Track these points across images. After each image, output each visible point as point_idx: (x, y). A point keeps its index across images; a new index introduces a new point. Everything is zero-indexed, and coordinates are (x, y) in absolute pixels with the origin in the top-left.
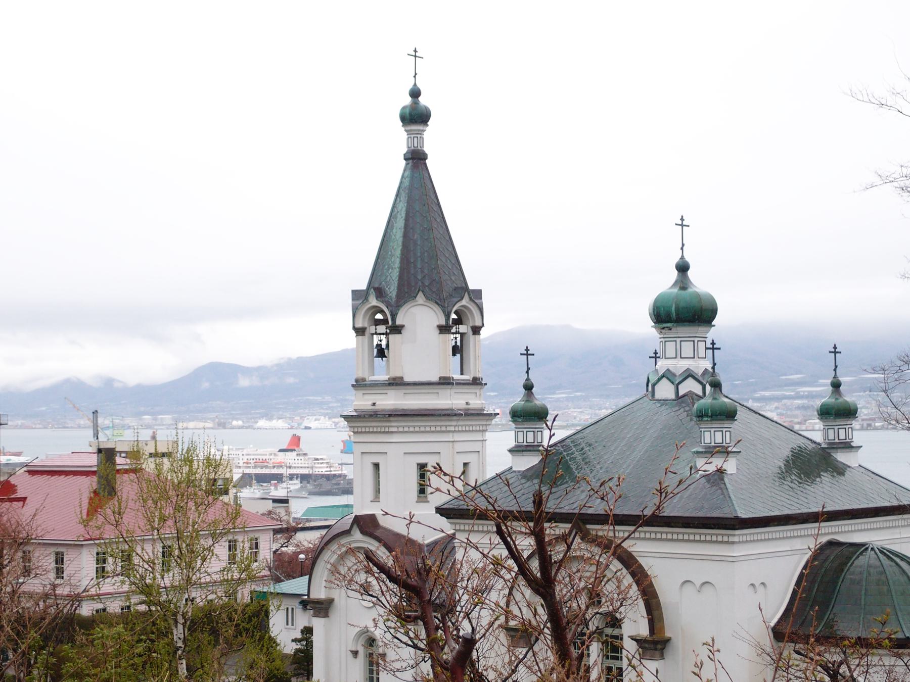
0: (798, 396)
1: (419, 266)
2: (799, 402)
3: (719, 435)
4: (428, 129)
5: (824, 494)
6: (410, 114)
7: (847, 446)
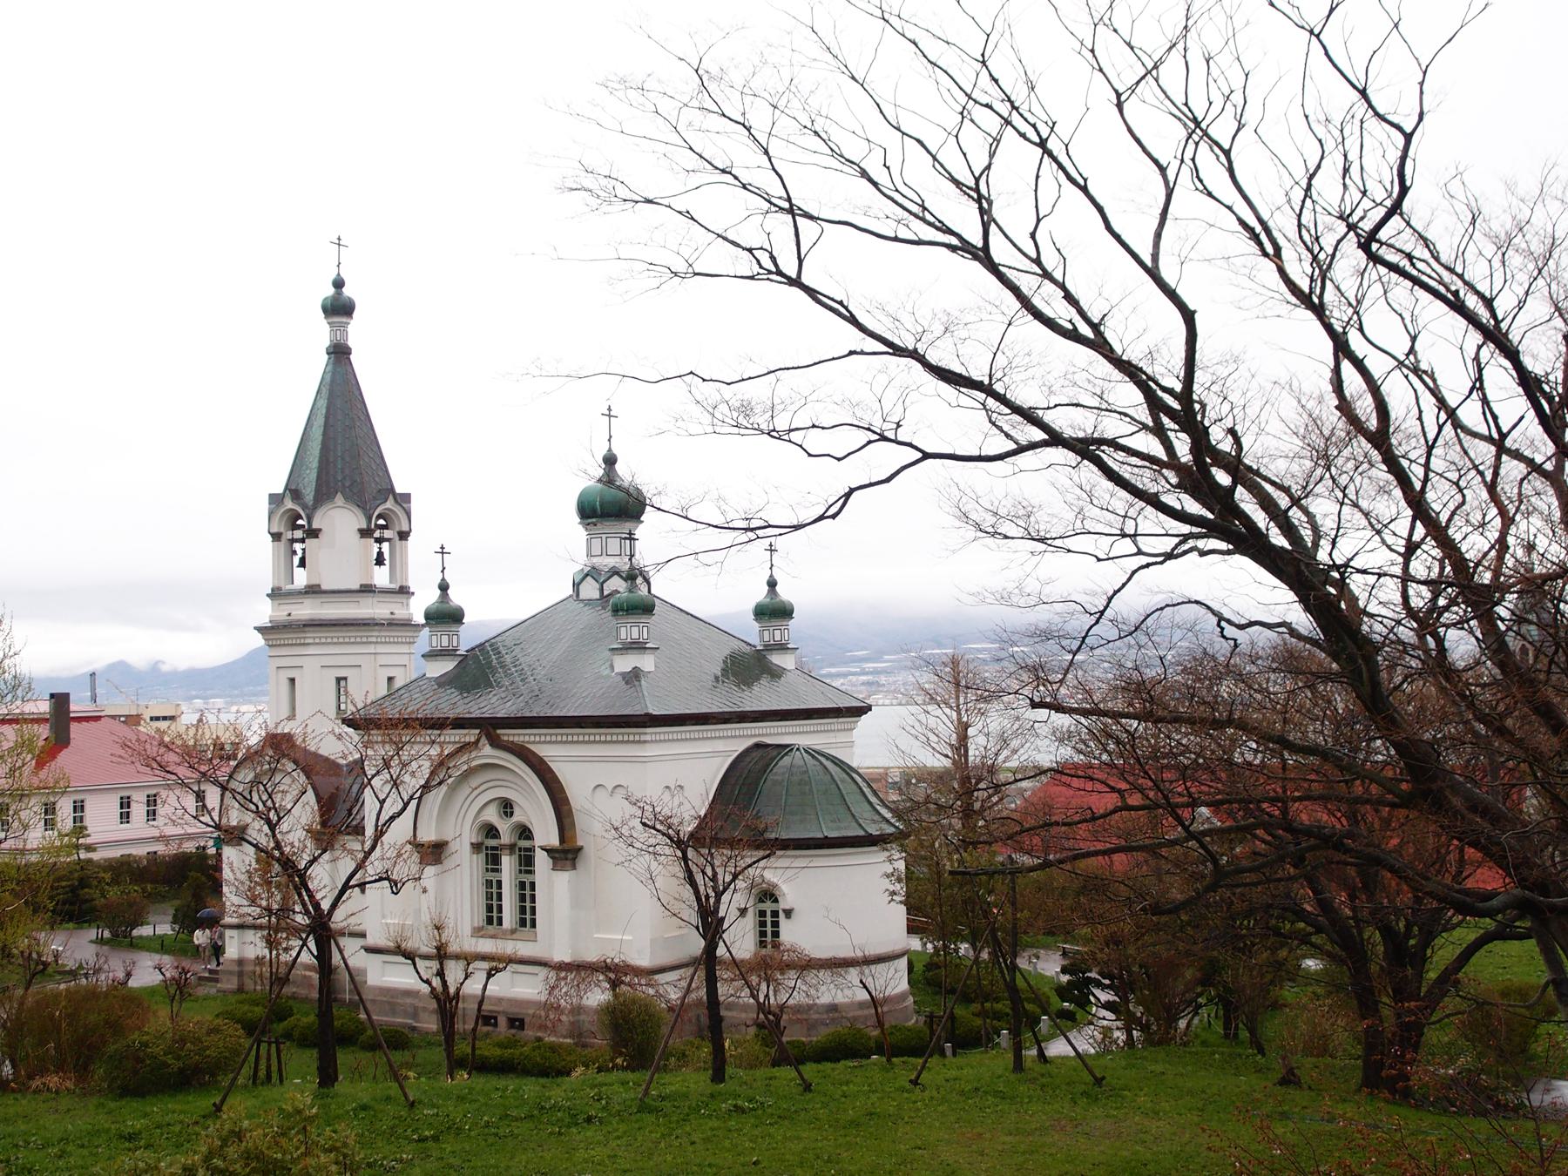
0: (864, 673)
1: (340, 468)
2: (864, 678)
3: (635, 630)
5: (761, 697)
7: (782, 647)
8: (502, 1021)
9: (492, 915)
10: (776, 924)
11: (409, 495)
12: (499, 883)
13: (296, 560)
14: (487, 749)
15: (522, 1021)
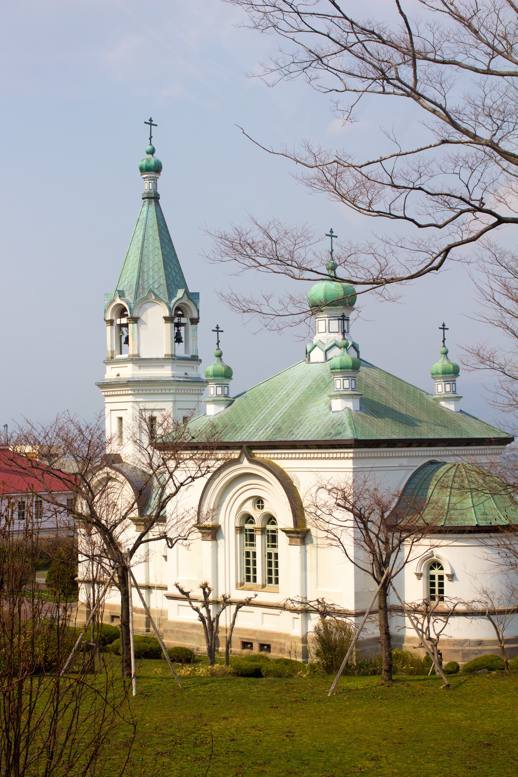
4: (160, 177)
6: (146, 166)
8: (256, 646)
9: (249, 575)
10: (441, 585)
11: (197, 294)
12: (254, 554)
13: (123, 340)
14: (246, 462)
15: (269, 646)
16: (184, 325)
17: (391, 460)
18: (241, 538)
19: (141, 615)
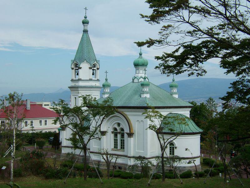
1: (84, 55)
8: (117, 168)
12: (117, 140)
13: (76, 74)
16: (95, 70)
17: (164, 112)
18: (113, 135)
19: (81, 157)
